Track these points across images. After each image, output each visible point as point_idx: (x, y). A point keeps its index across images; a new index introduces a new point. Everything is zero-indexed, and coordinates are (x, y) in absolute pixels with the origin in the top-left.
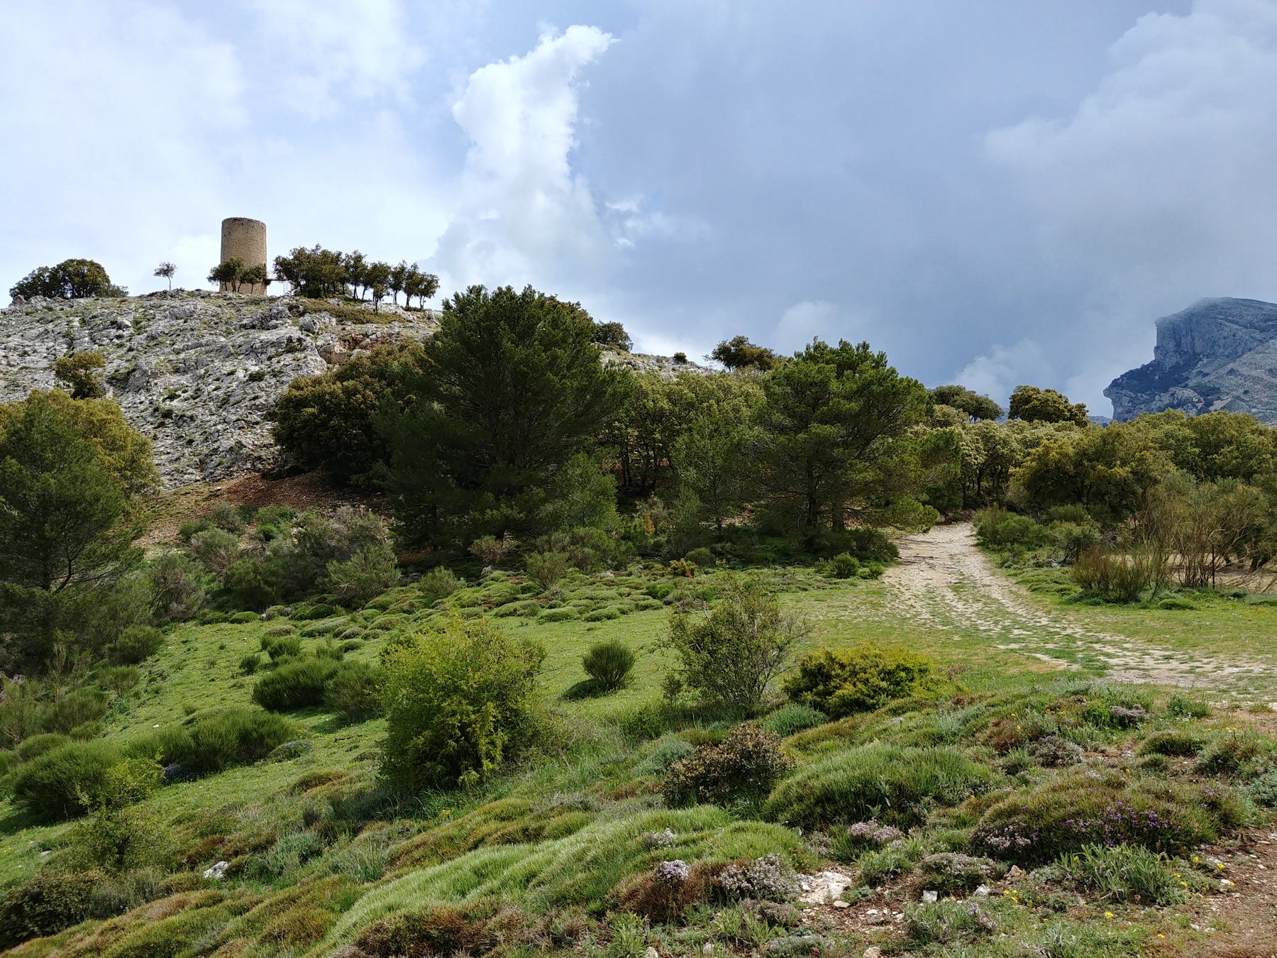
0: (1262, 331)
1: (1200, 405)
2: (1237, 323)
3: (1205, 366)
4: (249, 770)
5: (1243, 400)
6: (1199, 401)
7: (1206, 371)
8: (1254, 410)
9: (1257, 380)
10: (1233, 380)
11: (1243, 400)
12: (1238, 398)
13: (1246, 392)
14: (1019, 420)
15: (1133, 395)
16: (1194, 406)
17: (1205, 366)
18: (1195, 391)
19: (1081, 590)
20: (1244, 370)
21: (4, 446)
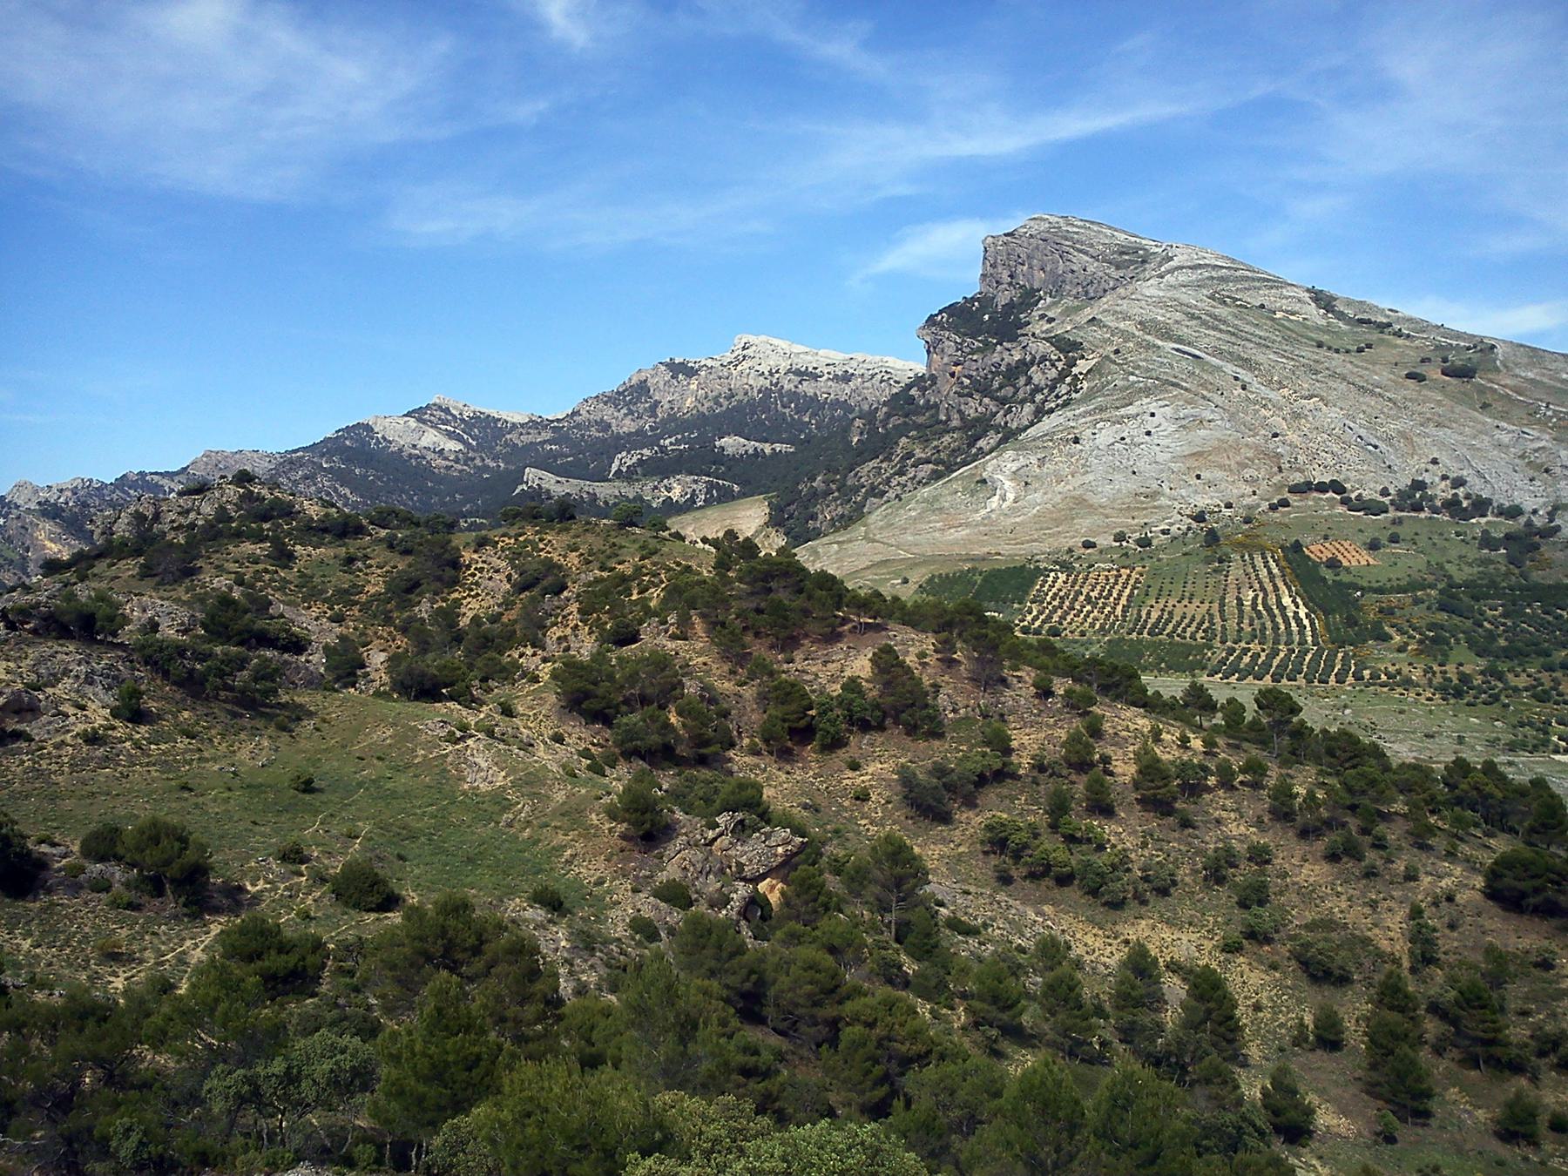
0: (1118, 268)
1: (1060, 365)
2: (1086, 253)
3: (1048, 308)
4: (1500, 1143)
5: (1114, 362)
6: (1059, 360)
7: (1050, 314)
8: (1132, 378)
9: (1127, 336)
10: (1097, 334)
11: (1114, 362)
12: (1107, 357)
13: (1117, 352)
14: (1327, 481)
15: (959, 340)
16: (1053, 365)
17: (1048, 308)
18: (1052, 344)
19: (461, 624)
20: (1108, 320)
21: (2, 1050)
